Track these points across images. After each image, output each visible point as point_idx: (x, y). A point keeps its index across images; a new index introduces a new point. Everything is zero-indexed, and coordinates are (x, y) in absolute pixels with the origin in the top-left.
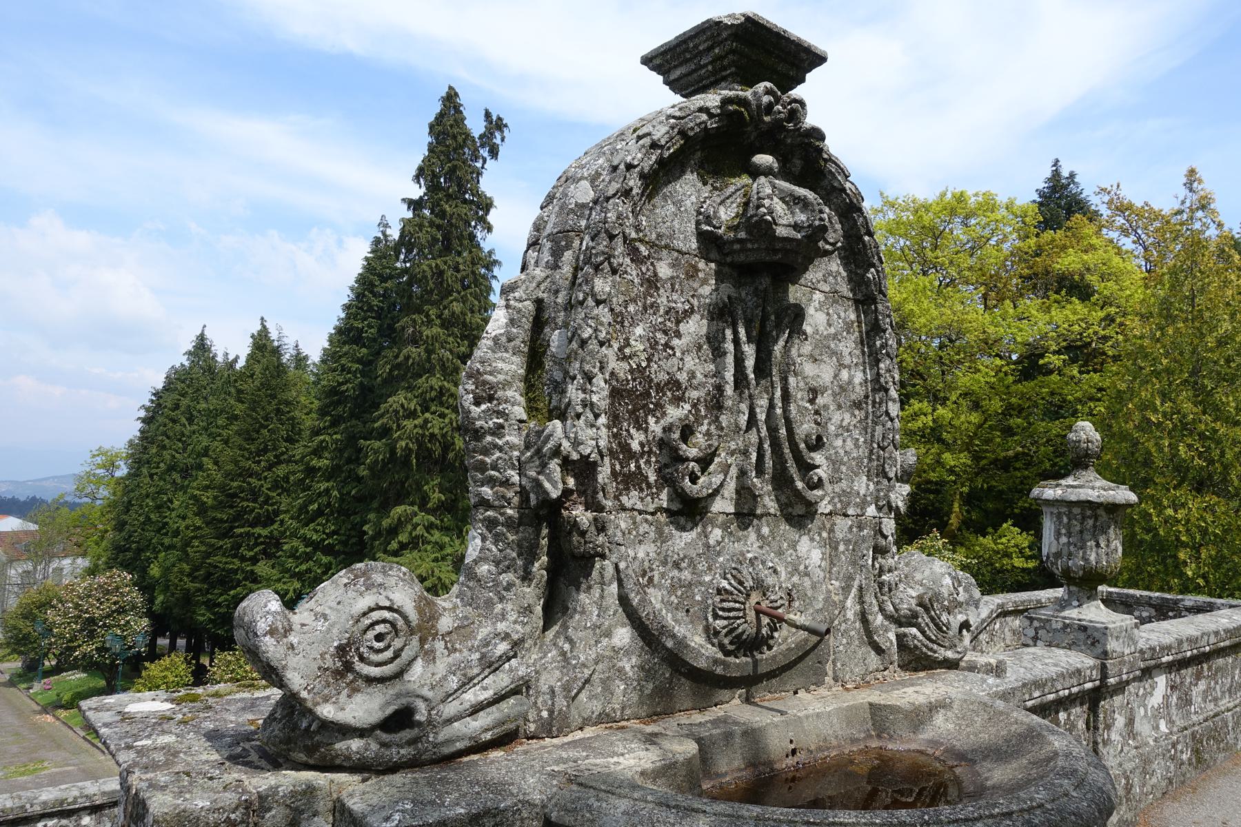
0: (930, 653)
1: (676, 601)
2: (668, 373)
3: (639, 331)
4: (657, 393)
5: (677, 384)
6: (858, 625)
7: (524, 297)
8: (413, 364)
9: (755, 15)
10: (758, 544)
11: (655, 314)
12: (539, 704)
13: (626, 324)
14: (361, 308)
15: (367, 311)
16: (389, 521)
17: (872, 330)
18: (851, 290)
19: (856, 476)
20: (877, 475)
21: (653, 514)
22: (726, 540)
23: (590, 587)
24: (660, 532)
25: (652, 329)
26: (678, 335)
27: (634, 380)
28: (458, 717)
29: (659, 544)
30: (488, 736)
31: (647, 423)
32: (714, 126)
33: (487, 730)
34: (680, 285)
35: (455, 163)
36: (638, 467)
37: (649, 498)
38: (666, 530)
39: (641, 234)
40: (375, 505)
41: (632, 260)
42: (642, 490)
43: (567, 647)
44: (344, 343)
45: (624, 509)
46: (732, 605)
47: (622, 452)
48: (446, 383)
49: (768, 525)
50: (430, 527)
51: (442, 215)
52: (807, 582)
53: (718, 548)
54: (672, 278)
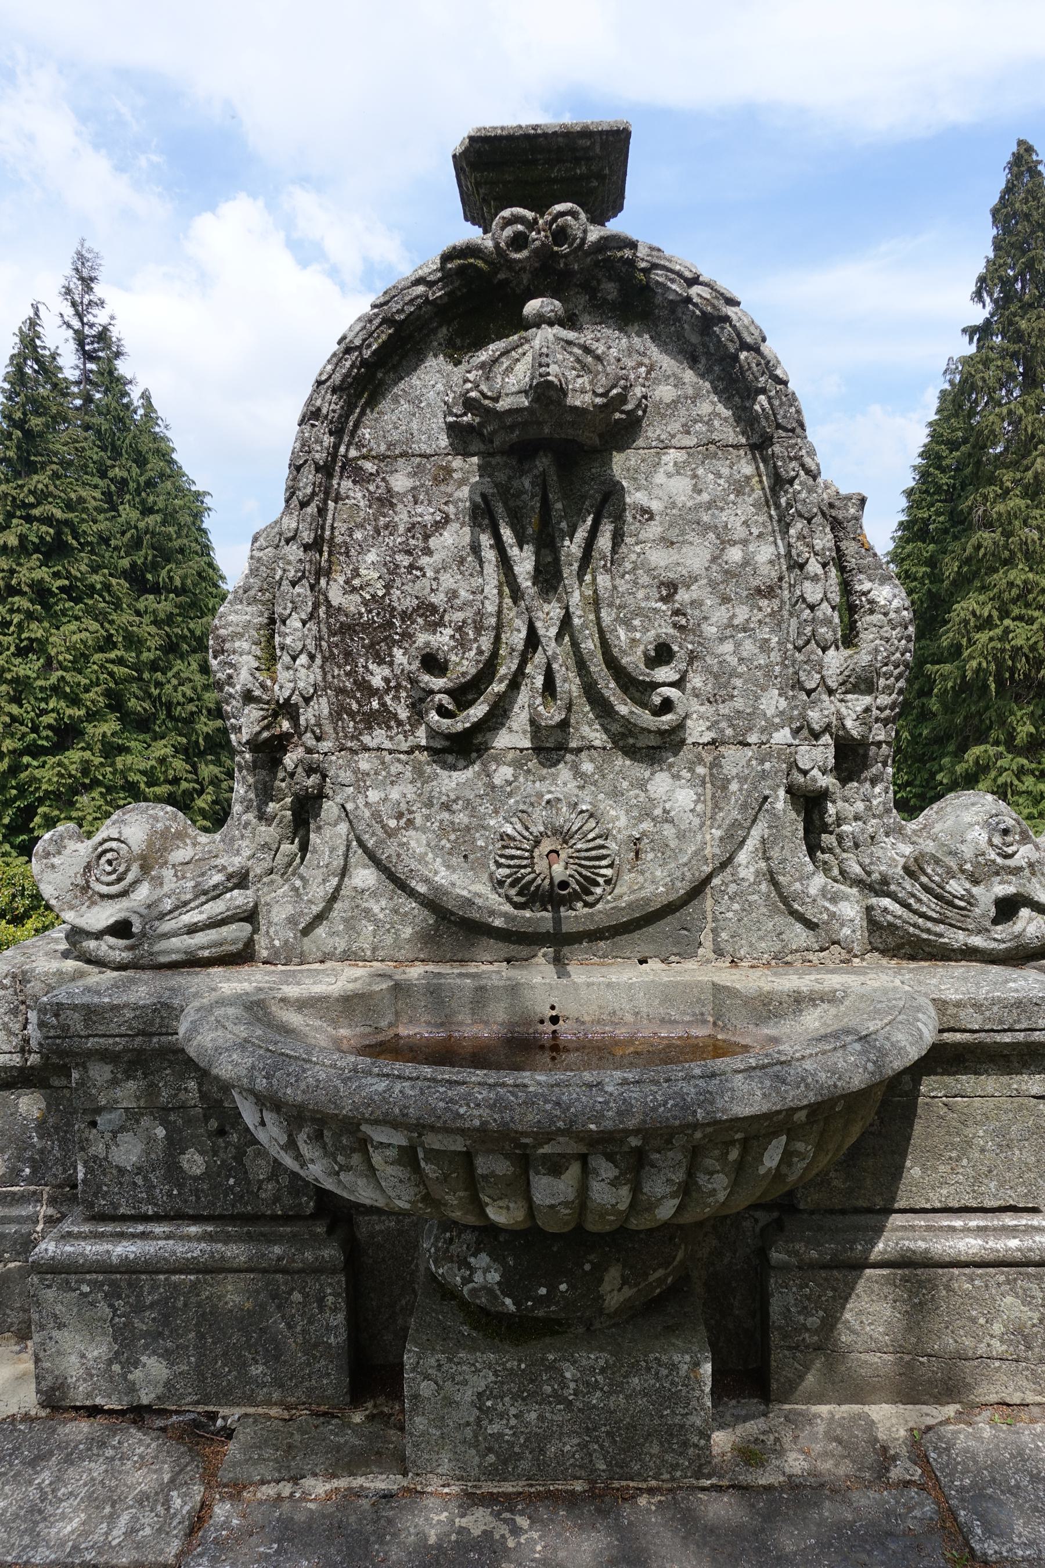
0: (925, 936)
1: (448, 845)
2: (417, 598)
3: (371, 557)
4: (403, 621)
5: (433, 609)
6: (764, 887)
7: (265, 544)
8: (985, 555)
9: (479, 130)
10: (575, 783)
11: (391, 534)
12: (272, 933)
13: (353, 552)
14: (926, 492)
15: (934, 493)
16: (965, 765)
17: (775, 484)
18: (743, 433)
19: (763, 690)
20: (793, 687)
21: (407, 753)
22: (521, 779)
23: (319, 828)
24: (419, 772)
25: (390, 552)
26: (428, 552)
27: (370, 612)
28: (175, 934)
29: (419, 785)
30: (206, 953)
31: (391, 655)
32: (439, 294)
33: (208, 947)
34: (427, 493)
35: (1031, 254)
36: (383, 704)
37: (401, 736)
38: (428, 769)
39: (364, 450)
40: (951, 748)
41: (354, 482)
42: (389, 728)
43: (298, 883)
44: (908, 541)
45: (367, 749)
46: (514, 852)
47: (358, 689)
48: (1031, 575)
49: (592, 761)
50: (1020, 773)
51: (1018, 336)
52: (669, 831)
53: (508, 789)
54: (414, 488)
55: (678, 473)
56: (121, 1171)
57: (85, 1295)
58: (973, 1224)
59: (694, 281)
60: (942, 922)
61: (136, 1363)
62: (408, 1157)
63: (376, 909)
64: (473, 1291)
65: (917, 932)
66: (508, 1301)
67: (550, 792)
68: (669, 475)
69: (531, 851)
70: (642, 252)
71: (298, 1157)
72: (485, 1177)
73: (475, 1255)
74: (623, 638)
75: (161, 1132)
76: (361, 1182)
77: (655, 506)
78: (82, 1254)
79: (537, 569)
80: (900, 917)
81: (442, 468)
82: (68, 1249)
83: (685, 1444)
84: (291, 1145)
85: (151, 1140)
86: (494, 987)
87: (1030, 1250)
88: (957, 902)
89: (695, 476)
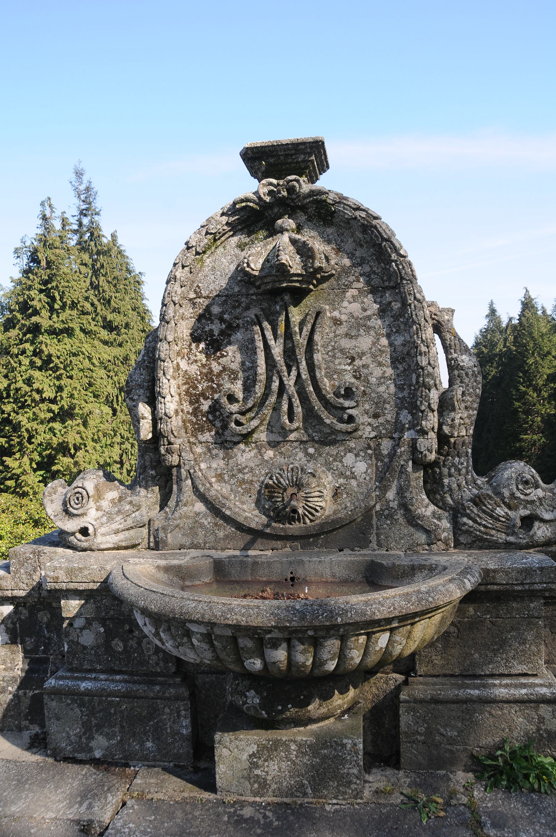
52: (354, 483)
55: (354, 301)
56: (85, 648)
57: (68, 705)
58: (504, 682)
59: (358, 209)
60: (494, 529)
61: (93, 738)
62: (208, 638)
63: (206, 523)
64: (248, 708)
65: (481, 534)
66: (263, 712)
67: (292, 463)
68: (350, 303)
69: (282, 494)
70: (331, 196)
71: (161, 640)
72: (242, 648)
73: (248, 691)
74: (328, 385)
75: (102, 630)
76: (188, 651)
77: (344, 318)
78: (67, 686)
79: (285, 351)
80: (472, 527)
81: (237, 301)
82: (61, 683)
83: (350, 782)
84: (157, 634)
85: (98, 633)
86: (262, 562)
87: (532, 694)
88: (501, 519)
89: (363, 302)
